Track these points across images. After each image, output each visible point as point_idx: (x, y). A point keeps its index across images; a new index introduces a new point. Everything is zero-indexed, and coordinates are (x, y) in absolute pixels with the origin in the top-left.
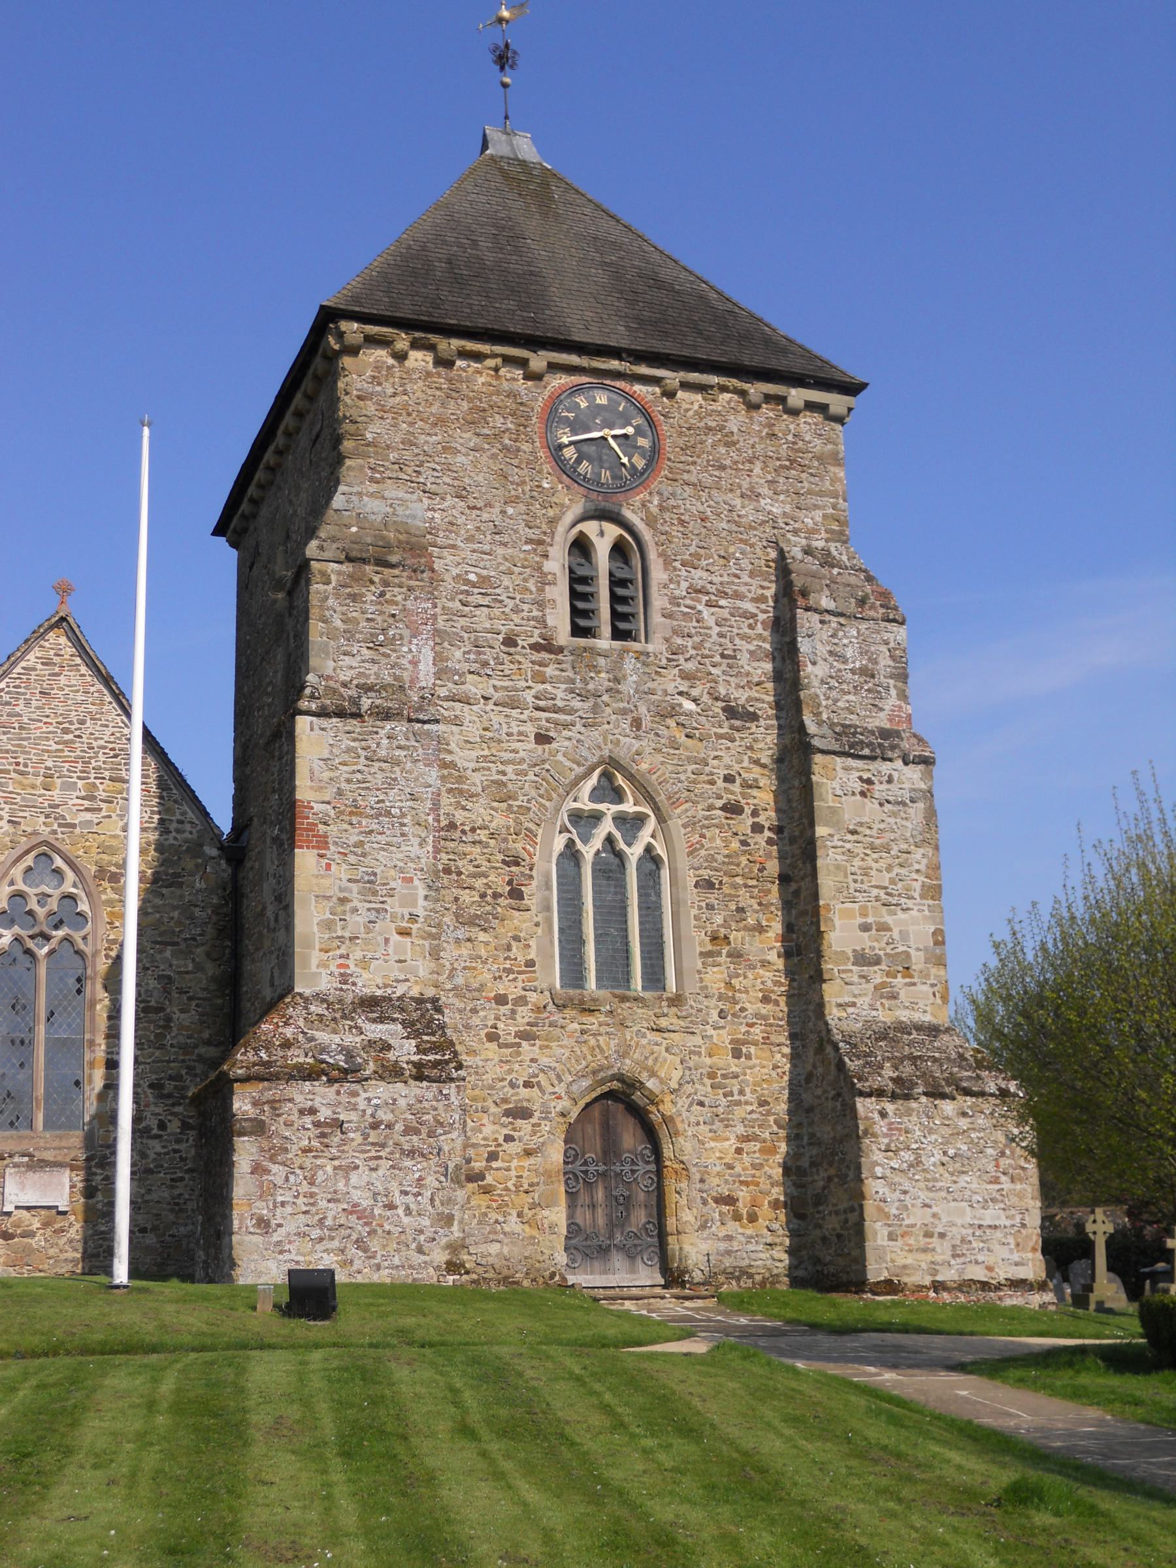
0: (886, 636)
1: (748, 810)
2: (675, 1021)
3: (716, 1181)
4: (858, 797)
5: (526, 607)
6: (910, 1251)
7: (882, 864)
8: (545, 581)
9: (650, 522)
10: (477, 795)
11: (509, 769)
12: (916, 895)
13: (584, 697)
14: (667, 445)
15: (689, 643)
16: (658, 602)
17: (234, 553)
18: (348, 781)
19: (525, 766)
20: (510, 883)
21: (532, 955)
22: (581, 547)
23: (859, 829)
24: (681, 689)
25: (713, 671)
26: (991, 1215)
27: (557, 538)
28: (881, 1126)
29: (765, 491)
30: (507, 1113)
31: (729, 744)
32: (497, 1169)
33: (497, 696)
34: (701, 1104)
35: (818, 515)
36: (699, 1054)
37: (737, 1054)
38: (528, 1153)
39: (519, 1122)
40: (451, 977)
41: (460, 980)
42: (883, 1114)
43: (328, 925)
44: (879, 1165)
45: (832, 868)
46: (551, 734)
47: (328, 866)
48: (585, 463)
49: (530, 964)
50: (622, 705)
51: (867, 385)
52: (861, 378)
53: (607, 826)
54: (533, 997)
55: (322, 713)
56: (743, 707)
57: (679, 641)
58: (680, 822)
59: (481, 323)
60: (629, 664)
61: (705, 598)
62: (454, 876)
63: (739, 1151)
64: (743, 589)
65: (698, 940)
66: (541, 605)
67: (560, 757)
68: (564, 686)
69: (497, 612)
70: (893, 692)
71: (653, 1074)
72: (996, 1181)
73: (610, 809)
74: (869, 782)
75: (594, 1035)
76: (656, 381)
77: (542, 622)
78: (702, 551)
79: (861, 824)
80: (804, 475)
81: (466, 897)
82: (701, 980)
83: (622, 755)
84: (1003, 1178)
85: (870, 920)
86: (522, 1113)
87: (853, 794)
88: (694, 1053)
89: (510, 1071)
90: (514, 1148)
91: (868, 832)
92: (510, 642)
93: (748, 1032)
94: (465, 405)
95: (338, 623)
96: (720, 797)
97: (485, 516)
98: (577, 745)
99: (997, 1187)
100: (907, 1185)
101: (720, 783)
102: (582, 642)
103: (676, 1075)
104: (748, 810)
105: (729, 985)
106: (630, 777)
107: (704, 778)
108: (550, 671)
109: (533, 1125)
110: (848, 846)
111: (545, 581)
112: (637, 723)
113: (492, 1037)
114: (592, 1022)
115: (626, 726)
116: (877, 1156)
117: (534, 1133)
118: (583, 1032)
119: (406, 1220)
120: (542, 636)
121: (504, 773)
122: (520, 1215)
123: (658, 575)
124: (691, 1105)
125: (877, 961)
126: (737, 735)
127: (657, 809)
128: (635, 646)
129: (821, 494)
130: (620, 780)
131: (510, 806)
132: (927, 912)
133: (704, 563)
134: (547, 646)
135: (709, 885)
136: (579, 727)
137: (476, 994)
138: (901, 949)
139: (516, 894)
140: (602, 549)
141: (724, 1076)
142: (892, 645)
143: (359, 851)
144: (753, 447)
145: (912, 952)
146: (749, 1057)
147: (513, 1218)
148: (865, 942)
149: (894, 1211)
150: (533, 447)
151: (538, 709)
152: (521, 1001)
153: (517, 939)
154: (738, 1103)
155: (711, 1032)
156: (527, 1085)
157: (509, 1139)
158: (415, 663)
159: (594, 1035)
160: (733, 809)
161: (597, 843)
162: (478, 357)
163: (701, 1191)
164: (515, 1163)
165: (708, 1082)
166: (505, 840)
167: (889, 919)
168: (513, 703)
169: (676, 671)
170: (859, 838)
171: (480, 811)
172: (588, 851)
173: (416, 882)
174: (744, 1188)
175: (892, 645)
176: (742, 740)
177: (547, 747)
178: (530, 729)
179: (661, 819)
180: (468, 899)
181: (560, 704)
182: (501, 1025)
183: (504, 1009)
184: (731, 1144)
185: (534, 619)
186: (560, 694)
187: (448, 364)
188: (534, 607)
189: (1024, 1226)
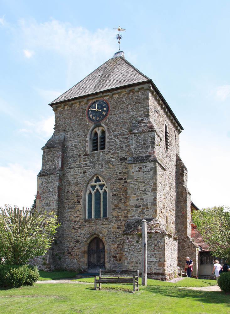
0: (149, 135)
1: (124, 179)
2: (107, 223)
3: (113, 253)
4: (138, 172)
5: (82, 148)
6: (132, 266)
7: (143, 185)
8: (86, 142)
9: (106, 125)
10: (72, 185)
11: (78, 179)
12: (150, 191)
15: (113, 147)
18: (45, 187)
19: (81, 178)
20: (78, 200)
21: (81, 213)
23: (138, 179)
24: (111, 157)
25: (118, 151)
27: (89, 133)
30: (75, 242)
31: (120, 166)
32: (73, 252)
33: (77, 166)
34: (110, 238)
35: (142, 112)
36: (111, 229)
37: (118, 228)
38: (78, 249)
39: (77, 243)
40: (67, 218)
41: (68, 219)
42: (128, 238)
44: (126, 249)
45: (130, 188)
46: (86, 171)
47: (41, 202)
48: (94, 117)
50: (99, 163)
51: (51, 105)
54: (81, 221)
56: (124, 157)
57: (111, 147)
58: (110, 184)
60: (101, 154)
61: (117, 137)
62: (68, 200)
63: (117, 247)
64: (125, 133)
66: (85, 147)
67: (88, 175)
68: (88, 162)
69: (77, 150)
70: (151, 147)
71: (101, 233)
72: (154, 251)
73: (97, 184)
74: (141, 168)
75: (91, 227)
78: (116, 128)
79: (138, 177)
80: (139, 105)
81: (70, 204)
82: (112, 214)
84: (156, 251)
85: (139, 198)
86: (78, 242)
87: (137, 171)
88: (110, 229)
89: (76, 234)
90: (76, 248)
91: (140, 179)
92: (80, 156)
93: (121, 224)
94: (74, 113)
95: (46, 160)
96: (118, 177)
97: (77, 133)
99: (154, 253)
100: (132, 253)
101: (118, 174)
104: (124, 179)
106: (101, 176)
107: (115, 174)
109: (80, 244)
110: (135, 183)
111: (86, 142)
112: (102, 166)
113: (73, 228)
115: (100, 166)
116: (127, 247)
117: (80, 245)
118: (89, 226)
119: (40, 260)
120: (85, 153)
121: (77, 180)
122: (76, 260)
124: (108, 239)
125: (140, 206)
126: (122, 164)
129: (143, 107)
131: (78, 186)
132: (152, 194)
133: (117, 130)
134: (86, 155)
135: (115, 195)
136: (92, 169)
137: (71, 221)
138: (146, 203)
139: (79, 202)
141: (116, 233)
142: (151, 136)
143: (46, 198)
144: (128, 102)
145: (148, 203)
146: (121, 228)
147: (75, 260)
148: (138, 203)
149: (129, 258)
151: (84, 167)
152: (79, 221)
153: (78, 210)
154: (118, 238)
155: (113, 224)
156: (79, 236)
157: (75, 246)
158: (58, 164)
159: (91, 227)
160: (121, 179)
162: (76, 103)
163: (109, 255)
164: (76, 250)
165: (112, 234)
166: (77, 193)
167: (143, 197)
168: (79, 167)
169: (110, 153)
170: (138, 181)
171: (73, 188)
173: (54, 203)
174: (118, 254)
175: (151, 136)
177: (85, 174)
178: (82, 171)
180: (70, 204)
181: (88, 165)
182: (75, 226)
183: (76, 223)
184: (116, 246)
185: (84, 150)
186: (88, 163)
188: (84, 148)
189: (160, 261)
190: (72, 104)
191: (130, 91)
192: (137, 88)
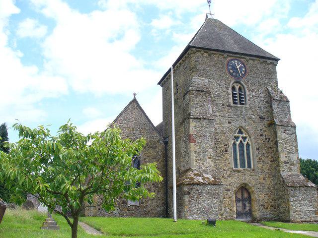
8: (229, 94)
13: (236, 115)
14: (226, 67)
16: (248, 98)
17: (162, 88)
22: (233, 88)
26: (311, 209)
28: (292, 192)
29: (264, 78)
43: (196, 157)
49: (229, 163)
51: (280, 59)
52: (279, 58)
53: (241, 139)
55: (194, 118)
59: (216, 48)
63: (265, 197)
65: (257, 159)
76: (245, 58)
77: (228, 102)
83: (243, 126)
98: (236, 124)
102: (235, 105)
103: (254, 183)
105: (262, 167)
106: (244, 129)
108: (230, 110)
111: (229, 94)
113: (223, 177)
114: (240, 174)
123: (247, 93)
125: (288, 163)
127: (249, 135)
128: (245, 106)
130: (243, 130)
134: (229, 106)
140: (237, 88)
147: (228, 209)
150: (225, 70)
160: (262, 135)
161: (239, 142)
172: (238, 143)
176: (263, 123)
178: (227, 121)
179: (250, 137)
187: (210, 55)
190: (212, 54)
191: (264, 61)
192: (269, 61)
